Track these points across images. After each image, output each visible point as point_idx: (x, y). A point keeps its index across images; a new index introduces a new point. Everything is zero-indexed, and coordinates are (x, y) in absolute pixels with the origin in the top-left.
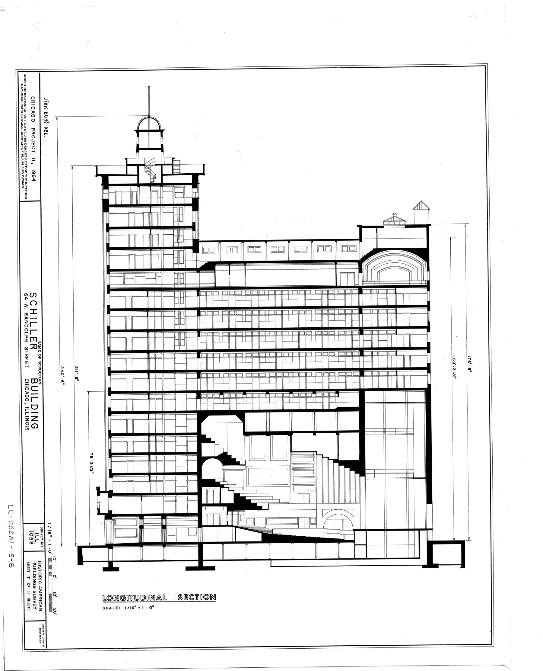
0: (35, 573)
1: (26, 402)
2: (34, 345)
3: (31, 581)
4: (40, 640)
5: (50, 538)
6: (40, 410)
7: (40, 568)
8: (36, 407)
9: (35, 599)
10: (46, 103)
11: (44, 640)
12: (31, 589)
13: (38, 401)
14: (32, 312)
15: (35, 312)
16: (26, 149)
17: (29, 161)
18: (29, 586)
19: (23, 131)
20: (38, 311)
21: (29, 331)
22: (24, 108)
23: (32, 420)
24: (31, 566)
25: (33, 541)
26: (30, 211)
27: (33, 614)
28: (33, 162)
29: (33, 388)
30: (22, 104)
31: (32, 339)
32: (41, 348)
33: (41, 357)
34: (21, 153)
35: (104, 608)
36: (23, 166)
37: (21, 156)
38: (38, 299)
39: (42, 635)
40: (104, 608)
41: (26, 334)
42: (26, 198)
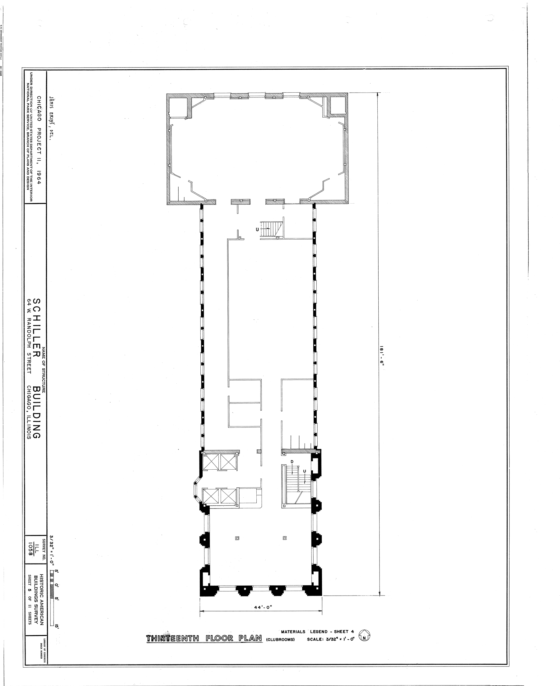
0: (36, 586)
1: (28, 410)
2: (37, 352)
3: (32, 594)
4: (41, 656)
5: (52, 550)
6: (43, 418)
7: (42, 581)
8: (38, 415)
9: (36, 613)
10: (52, 100)
11: (45, 655)
12: (33, 603)
13: (41, 410)
14: (35, 318)
15: (39, 318)
16: (31, 149)
17: (35, 160)
18: (30, 600)
19: (29, 131)
20: (42, 318)
21: (32, 337)
22: (30, 108)
23: (34, 430)
24: (33, 579)
25: (32, 552)
26: (35, 213)
27: (35, 628)
28: (38, 162)
29: (35, 396)
30: (28, 104)
31: (35, 346)
32: (45, 354)
33: (45, 363)
34: (26, 153)
35: (308, 639)
36: (28, 167)
37: (26, 156)
38: (42, 305)
39: (43, 650)
40: (308, 639)
41: (29, 340)
42: (31, 200)
